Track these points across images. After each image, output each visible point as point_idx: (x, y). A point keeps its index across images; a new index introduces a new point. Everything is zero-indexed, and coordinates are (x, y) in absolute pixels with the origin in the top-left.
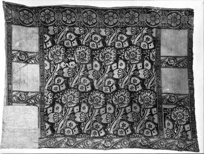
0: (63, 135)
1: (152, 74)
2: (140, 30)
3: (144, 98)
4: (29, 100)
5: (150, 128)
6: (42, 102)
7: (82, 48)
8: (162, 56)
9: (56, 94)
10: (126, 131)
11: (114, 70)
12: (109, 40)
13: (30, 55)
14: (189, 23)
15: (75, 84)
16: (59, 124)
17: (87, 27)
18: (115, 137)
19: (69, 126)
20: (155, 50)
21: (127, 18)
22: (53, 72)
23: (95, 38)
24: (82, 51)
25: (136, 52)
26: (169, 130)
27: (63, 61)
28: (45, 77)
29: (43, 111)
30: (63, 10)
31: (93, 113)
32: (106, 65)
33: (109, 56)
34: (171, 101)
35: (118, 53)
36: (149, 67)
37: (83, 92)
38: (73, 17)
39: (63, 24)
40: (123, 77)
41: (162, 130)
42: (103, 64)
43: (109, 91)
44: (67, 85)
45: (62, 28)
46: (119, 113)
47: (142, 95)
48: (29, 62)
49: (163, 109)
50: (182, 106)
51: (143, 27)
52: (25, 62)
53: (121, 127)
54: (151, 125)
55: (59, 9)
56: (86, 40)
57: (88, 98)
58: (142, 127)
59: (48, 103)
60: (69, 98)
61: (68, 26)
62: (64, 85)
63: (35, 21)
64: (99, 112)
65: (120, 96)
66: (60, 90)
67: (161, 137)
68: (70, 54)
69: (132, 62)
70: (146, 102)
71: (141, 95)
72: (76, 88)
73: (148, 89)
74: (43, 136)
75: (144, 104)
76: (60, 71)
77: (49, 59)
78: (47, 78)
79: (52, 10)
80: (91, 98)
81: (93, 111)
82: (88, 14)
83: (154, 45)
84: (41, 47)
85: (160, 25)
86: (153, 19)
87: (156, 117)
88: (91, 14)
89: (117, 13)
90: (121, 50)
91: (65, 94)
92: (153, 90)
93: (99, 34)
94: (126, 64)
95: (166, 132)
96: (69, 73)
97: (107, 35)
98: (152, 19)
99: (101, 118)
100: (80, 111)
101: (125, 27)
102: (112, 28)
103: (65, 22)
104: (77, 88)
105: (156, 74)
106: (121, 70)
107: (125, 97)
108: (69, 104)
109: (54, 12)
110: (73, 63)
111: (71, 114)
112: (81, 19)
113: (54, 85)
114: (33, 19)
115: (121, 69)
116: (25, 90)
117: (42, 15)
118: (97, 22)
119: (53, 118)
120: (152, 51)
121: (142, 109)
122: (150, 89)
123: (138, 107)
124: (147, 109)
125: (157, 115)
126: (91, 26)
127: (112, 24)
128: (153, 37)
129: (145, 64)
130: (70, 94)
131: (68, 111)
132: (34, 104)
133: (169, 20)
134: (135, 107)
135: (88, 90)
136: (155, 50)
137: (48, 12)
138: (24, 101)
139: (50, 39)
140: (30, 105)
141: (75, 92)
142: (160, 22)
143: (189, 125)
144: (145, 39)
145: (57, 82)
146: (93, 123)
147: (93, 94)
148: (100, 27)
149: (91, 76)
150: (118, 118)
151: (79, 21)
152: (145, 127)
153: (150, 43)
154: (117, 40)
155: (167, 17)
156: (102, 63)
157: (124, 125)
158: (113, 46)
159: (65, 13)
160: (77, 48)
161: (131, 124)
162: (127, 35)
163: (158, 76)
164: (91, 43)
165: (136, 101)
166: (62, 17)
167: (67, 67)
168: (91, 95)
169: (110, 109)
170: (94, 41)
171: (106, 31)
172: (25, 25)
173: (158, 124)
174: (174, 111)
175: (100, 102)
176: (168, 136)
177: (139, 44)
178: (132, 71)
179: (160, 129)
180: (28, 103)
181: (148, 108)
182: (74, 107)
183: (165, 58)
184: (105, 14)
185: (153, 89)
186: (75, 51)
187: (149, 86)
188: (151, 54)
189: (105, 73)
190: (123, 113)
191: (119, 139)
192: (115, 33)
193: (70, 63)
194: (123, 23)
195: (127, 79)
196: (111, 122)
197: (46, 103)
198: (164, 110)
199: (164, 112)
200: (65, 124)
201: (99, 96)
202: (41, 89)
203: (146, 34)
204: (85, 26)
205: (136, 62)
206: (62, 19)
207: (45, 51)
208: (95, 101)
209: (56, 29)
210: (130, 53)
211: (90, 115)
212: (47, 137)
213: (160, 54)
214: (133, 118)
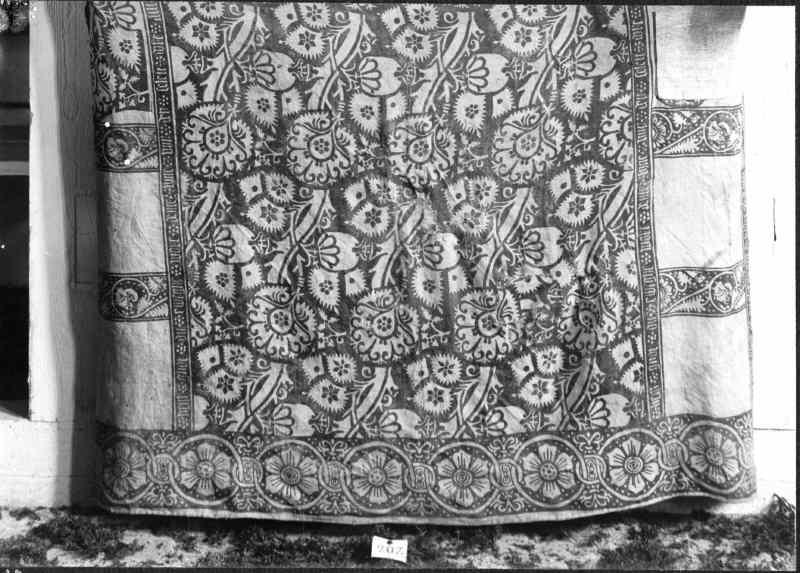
1: (202, 245)
2: (255, 421)
3: (229, 144)
4: (693, 125)
5: (201, 25)
7: (494, 353)
9: (590, 152)
10: (217, 362)
12: (381, 391)
15: (512, 205)
16: (572, 32)
17: (473, 439)
19: (529, 32)
20: (194, 342)
22: (603, 241)
24: (493, 340)
25: (271, 332)
26: (125, 25)
28: (634, 218)
29: (637, 81)
30: (574, 497)
31: (432, 95)
32: (390, 291)
33: (379, 327)
35: (345, 337)
36: (214, 269)
41: (151, 21)
44: (544, 193)
45: (575, 422)
47: (237, 157)
48: (699, 275)
49: (151, 104)
51: (247, 433)
52: (712, 274)
53: (320, 35)
54: (195, 35)
55: (589, 498)
56: (515, 207)
59: (617, 114)
60: (533, 145)
61: (551, 433)
62: (557, 192)
65: (328, 159)
66: (573, 172)
68: (540, 322)
70: (223, 130)
71: (242, 158)
72: (508, 186)
73: (214, 180)
75: (229, 119)
77: (620, 291)
78: (625, 216)
79: (617, 494)
80: (445, 153)
82: (472, 492)
84: (654, 343)
85: (177, 445)
86: (205, 467)
87: (179, 72)
88: (458, 495)
89: (351, 498)
90: (331, 344)
91: (551, 156)
92: (194, 181)
93: (425, 415)
94: (306, 288)
95: (135, 15)
97: (391, 411)
98: (210, 469)
100: (489, 96)
101: (317, 437)
102: (372, 440)
104: (502, 190)
105: (185, 247)
107: (308, 154)
108: (533, 121)
109: (608, 488)
110: (523, 288)
111: (524, 82)
113: (596, 191)
114: (687, 446)
117: (654, 466)
118: (433, 464)
119: (596, 55)
120: (205, 339)
121: (237, 100)
122: (205, 184)
123: (252, 107)
124: (215, 102)
125: (176, 81)
126: (459, 444)
130: (530, 161)
131: (539, 88)
132: (671, 107)
136: (194, 342)
137: (634, 484)
138: (712, 120)
139: (621, 374)
140: (688, 103)
141: (510, 173)
142: (175, 458)
144: (236, 386)
145: (583, 200)
146: (432, 56)
148: (419, 444)
151: (508, 460)
152: (219, 27)
153: (214, 369)
154: (350, 387)
159: (564, 485)
160: (510, 348)
161: (275, 43)
163: (177, 236)
164: (455, 376)
165: (261, 135)
166: (574, 467)
167: (547, 269)
168: (445, 165)
170: (445, 385)
173: (167, 45)
175: (407, 140)
177: (258, 364)
179: (160, 23)
180: (699, 113)
181: (211, 103)
182: (512, 112)
185: (195, 184)
186: (521, 335)
187: (209, 197)
188: (208, 325)
189: (390, 260)
190: (313, 89)
198: (147, 101)
199: (147, 96)
200: (547, 35)
201: (411, 166)
202: (649, 169)
204: (481, 444)
206: (578, 460)
207: (638, 326)
209: (595, 416)
211: (447, 85)
213: (174, 330)
214: (269, 64)
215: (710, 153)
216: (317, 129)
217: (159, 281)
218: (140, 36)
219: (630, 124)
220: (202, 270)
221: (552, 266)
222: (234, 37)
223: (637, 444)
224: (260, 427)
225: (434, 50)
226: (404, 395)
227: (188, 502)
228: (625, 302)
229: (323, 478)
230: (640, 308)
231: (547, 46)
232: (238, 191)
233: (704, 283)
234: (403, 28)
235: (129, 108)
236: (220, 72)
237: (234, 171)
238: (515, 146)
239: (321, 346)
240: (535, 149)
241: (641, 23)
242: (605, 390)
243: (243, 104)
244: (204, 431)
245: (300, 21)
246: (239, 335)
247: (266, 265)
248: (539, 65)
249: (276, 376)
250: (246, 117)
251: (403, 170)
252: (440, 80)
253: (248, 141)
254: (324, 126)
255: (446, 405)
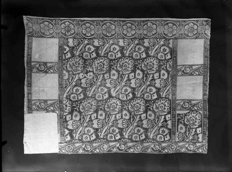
0: (81, 140)
2: (158, 41)
6: (61, 109)
8: (179, 66)
11: (132, 79)
13: (49, 65)
14: (206, 32)
15: (93, 93)
17: (106, 39)
18: (129, 141)
21: (145, 30)
23: (113, 48)
27: (81, 72)
32: (124, 73)
34: (185, 107)
35: (147, 104)
37: (100, 101)
38: (93, 30)
39: (83, 36)
40: (140, 86)
41: (174, 134)
42: (121, 73)
43: (125, 99)
46: (135, 120)
50: (195, 110)
51: (160, 39)
52: (45, 72)
54: (165, 131)
57: (105, 106)
58: (156, 133)
59: (67, 111)
63: (56, 33)
64: (115, 117)
67: (173, 141)
69: (149, 73)
73: (163, 98)
74: (63, 141)
76: (78, 81)
77: (68, 70)
78: (66, 87)
79: (72, 22)
81: (109, 118)
83: (171, 55)
84: (60, 58)
85: (177, 36)
87: (169, 123)
94: (144, 74)
96: (87, 83)
99: (117, 123)
101: (143, 39)
102: (130, 39)
103: (85, 35)
106: (138, 79)
107: (140, 105)
110: (91, 74)
111: (89, 121)
112: (101, 32)
114: (53, 30)
115: (138, 78)
116: (45, 98)
119: (72, 125)
121: (156, 116)
123: (153, 115)
124: (162, 116)
127: (130, 35)
128: (170, 48)
129: (162, 73)
132: (53, 111)
133: (186, 31)
134: (150, 114)
135: (105, 98)
138: (43, 108)
139: (69, 51)
141: (93, 100)
143: (201, 128)
147: (110, 101)
149: (108, 85)
150: (133, 124)
154: (135, 51)
155: (184, 28)
156: (187, 126)
157: (139, 131)
158: (130, 57)
160: (96, 60)
161: (146, 130)
162: (144, 47)
165: (151, 108)
167: (85, 77)
169: (126, 115)
171: (124, 42)
172: (46, 36)
174: (187, 116)
176: (180, 139)
178: (149, 80)
181: (151, 74)
183: (181, 67)
184: (123, 26)
191: (132, 144)
192: (133, 44)
193: (88, 74)
194: (141, 34)
195: (143, 88)
196: (127, 127)
197: (65, 110)
202: (59, 97)
203: (163, 45)
205: (153, 72)
206: (81, 32)
207: (64, 61)
208: (112, 107)
210: (148, 63)
211: (107, 121)
212: (66, 142)
213: (176, 63)
215: (44, 100)
216: (138, 110)
217: (179, 74)
218: (178, 131)
219: (64, 108)
220: (168, 77)
221: (84, 78)
222: (156, 131)
223: (67, 33)
224: (157, 40)
225: (109, 129)
226: (122, 49)
227: (175, 22)
228: (66, 67)
229: (142, 29)
230: (63, 66)
231: (83, 129)
232: (158, 95)
233: (47, 70)
234: (116, 135)
235: (182, 114)
236: (160, 122)
237: (147, 59)
238: (91, 106)
239: (141, 61)
240: (87, 105)
241: (61, 131)
242: (73, 47)
243: (155, 115)
244: (170, 39)
245: (140, 135)
246: (161, 62)
247: (153, 78)
248: (85, 124)
249: (152, 53)
250: (154, 112)
251: (118, 102)
252: (108, 122)
253: (154, 107)
254: (136, 111)
255: (112, 47)
